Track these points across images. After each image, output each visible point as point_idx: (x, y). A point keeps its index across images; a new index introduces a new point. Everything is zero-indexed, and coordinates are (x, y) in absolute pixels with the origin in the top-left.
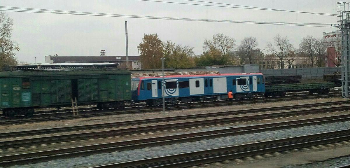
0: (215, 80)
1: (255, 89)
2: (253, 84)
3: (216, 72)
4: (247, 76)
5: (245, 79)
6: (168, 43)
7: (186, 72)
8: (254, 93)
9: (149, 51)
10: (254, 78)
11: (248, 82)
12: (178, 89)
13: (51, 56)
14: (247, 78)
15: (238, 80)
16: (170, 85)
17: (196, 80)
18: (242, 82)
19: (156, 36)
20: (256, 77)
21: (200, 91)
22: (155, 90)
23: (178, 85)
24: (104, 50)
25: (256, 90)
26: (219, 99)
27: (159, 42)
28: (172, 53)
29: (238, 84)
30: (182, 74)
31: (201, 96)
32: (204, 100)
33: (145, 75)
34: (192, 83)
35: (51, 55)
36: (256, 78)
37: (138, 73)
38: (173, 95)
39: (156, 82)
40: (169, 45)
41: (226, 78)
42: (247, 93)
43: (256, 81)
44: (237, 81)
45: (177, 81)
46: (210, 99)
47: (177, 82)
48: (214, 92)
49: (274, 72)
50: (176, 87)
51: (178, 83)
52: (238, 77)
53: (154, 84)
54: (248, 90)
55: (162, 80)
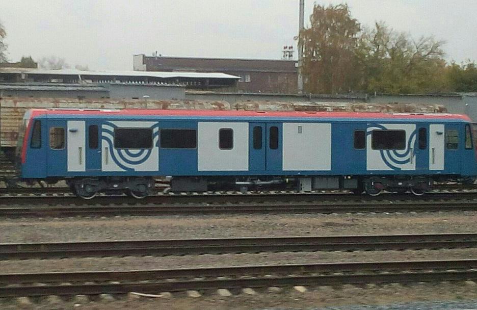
0: (288, 132)
1: (437, 164)
2: (431, 150)
3: (437, 107)
4: (409, 123)
5: (403, 133)
6: (378, 27)
7: (343, 104)
8: (437, 176)
9: (324, 50)
10: (433, 129)
11: (411, 140)
12: (155, 150)
13: (144, 56)
14: (409, 129)
15: (374, 133)
16: (129, 139)
17: (271, 126)
18: (389, 140)
19: (345, 10)
20: (443, 126)
21: (237, 160)
22: (78, 150)
23: (156, 139)
24: (290, 46)
25: (442, 168)
26: (306, 188)
27: (352, 26)
28: (388, 56)
29: (375, 147)
30: (329, 109)
31: (241, 176)
32: (250, 188)
33: (220, 107)
34: (207, 135)
35: (142, 53)
36: (443, 131)
37: (200, 101)
38: (138, 168)
39: (81, 126)
40: (381, 34)
41: (84, 122)
42: (407, 176)
43: (442, 139)
44: (369, 138)
45: (155, 126)
46: (271, 187)
47: (156, 130)
48: (68, 168)
49: (56, 105)
50: (149, 145)
51: (156, 134)
52: (374, 124)
53: (73, 131)
54: (411, 167)
55: (104, 121)
